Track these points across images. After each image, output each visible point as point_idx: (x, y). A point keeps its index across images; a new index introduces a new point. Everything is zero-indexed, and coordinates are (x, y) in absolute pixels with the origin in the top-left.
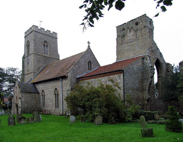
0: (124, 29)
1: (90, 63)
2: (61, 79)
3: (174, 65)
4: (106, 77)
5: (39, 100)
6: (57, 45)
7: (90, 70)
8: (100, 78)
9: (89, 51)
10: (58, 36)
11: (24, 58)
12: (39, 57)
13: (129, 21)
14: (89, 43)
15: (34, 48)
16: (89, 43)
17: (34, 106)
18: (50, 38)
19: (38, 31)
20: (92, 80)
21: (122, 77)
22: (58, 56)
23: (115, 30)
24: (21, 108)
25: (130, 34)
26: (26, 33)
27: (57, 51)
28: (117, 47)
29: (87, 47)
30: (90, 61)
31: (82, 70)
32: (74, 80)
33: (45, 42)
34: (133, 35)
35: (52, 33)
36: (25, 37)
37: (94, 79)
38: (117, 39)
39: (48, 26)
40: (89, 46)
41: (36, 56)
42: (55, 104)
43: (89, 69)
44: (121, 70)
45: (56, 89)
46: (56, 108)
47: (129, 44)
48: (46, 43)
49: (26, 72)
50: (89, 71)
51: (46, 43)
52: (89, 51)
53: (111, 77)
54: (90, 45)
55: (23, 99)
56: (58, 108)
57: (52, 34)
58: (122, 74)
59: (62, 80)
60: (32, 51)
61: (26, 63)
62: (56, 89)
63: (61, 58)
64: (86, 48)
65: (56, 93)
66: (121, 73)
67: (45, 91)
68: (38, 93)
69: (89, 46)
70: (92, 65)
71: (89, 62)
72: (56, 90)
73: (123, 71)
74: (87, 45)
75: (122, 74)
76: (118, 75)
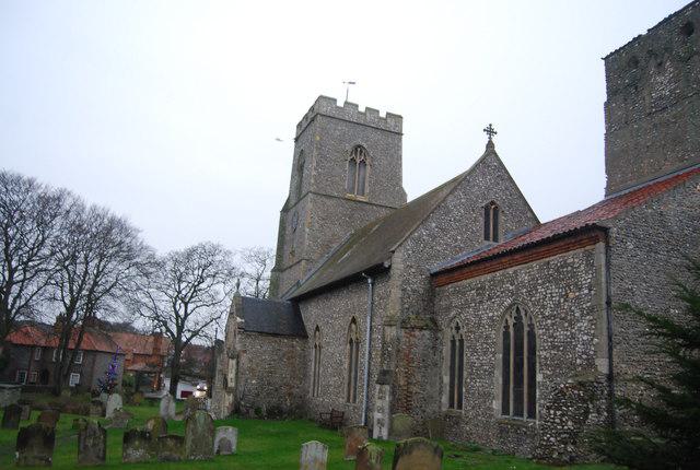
0: (635, 62)
1: (491, 212)
2: (370, 281)
3: (651, 384)
4: (535, 265)
5: (305, 365)
6: (400, 158)
7: (491, 243)
8: (510, 271)
9: (490, 163)
10: (407, 128)
11: (285, 210)
12: (329, 202)
13: (655, 23)
14: (490, 131)
15: (314, 173)
16: (490, 131)
17: (284, 390)
18: (375, 136)
19: (334, 113)
20: (483, 278)
21: (600, 259)
22: (404, 195)
23: (601, 67)
24: (235, 396)
25: (659, 79)
26: (299, 125)
27: (400, 179)
28: (606, 139)
29: (484, 149)
30: (492, 203)
31: (456, 240)
32: (418, 284)
33: (358, 149)
34: (676, 79)
35: (361, 113)
36: (296, 140)
37: (489, 277)
38: (607, 105)
39: (371, 96)
40: (490, 145)
41: (320, 200)
42: (346, 381)
43: (487, 238)
44: (594, 227)
45: (354, 321)
46: (348, 401)
47: (656, 120)
48: (361, 151)
49: (286, 262)
50: (487, 243)
51: (361, 151)
52: (490, 163)
53: (555, 260)
54: (495, 139)
55: (244, 359)
56: (460, 407)
57: (365, 114)
58: (601, 246)
59: (373, 284)
60: (310, 184)
61: (289, 229)
62: (354, 321)
63: (410, 199)
64: (481, 151)
65: (354, 338)
66: (595, 241)
67: (324, 330)
68: (304, 336)
69: (490, 145)
70: (502, 218)
71: (487, 209)
72: (353, 326)
73: (605, 230)
74: (485, 138)
75: (601, 246)
76: (580, 251)
